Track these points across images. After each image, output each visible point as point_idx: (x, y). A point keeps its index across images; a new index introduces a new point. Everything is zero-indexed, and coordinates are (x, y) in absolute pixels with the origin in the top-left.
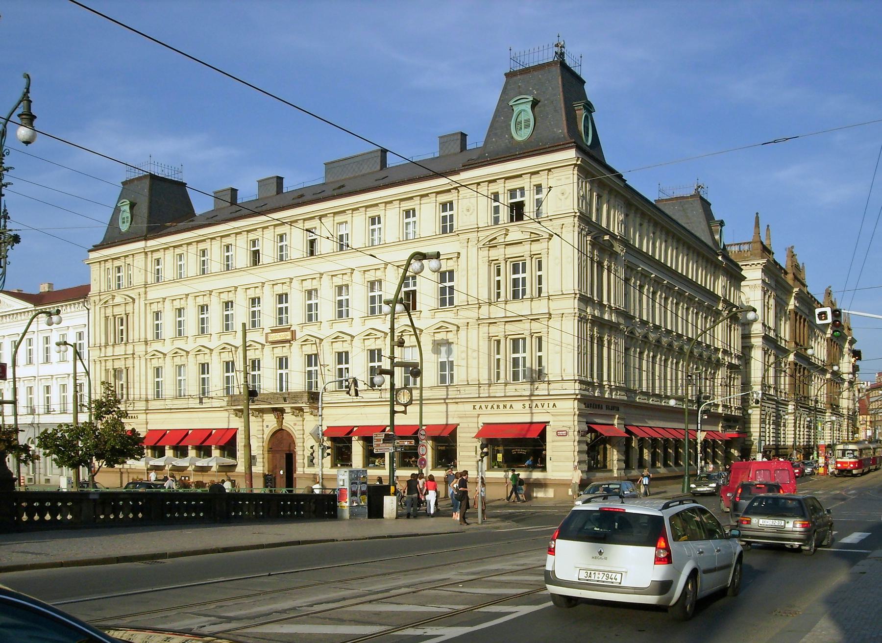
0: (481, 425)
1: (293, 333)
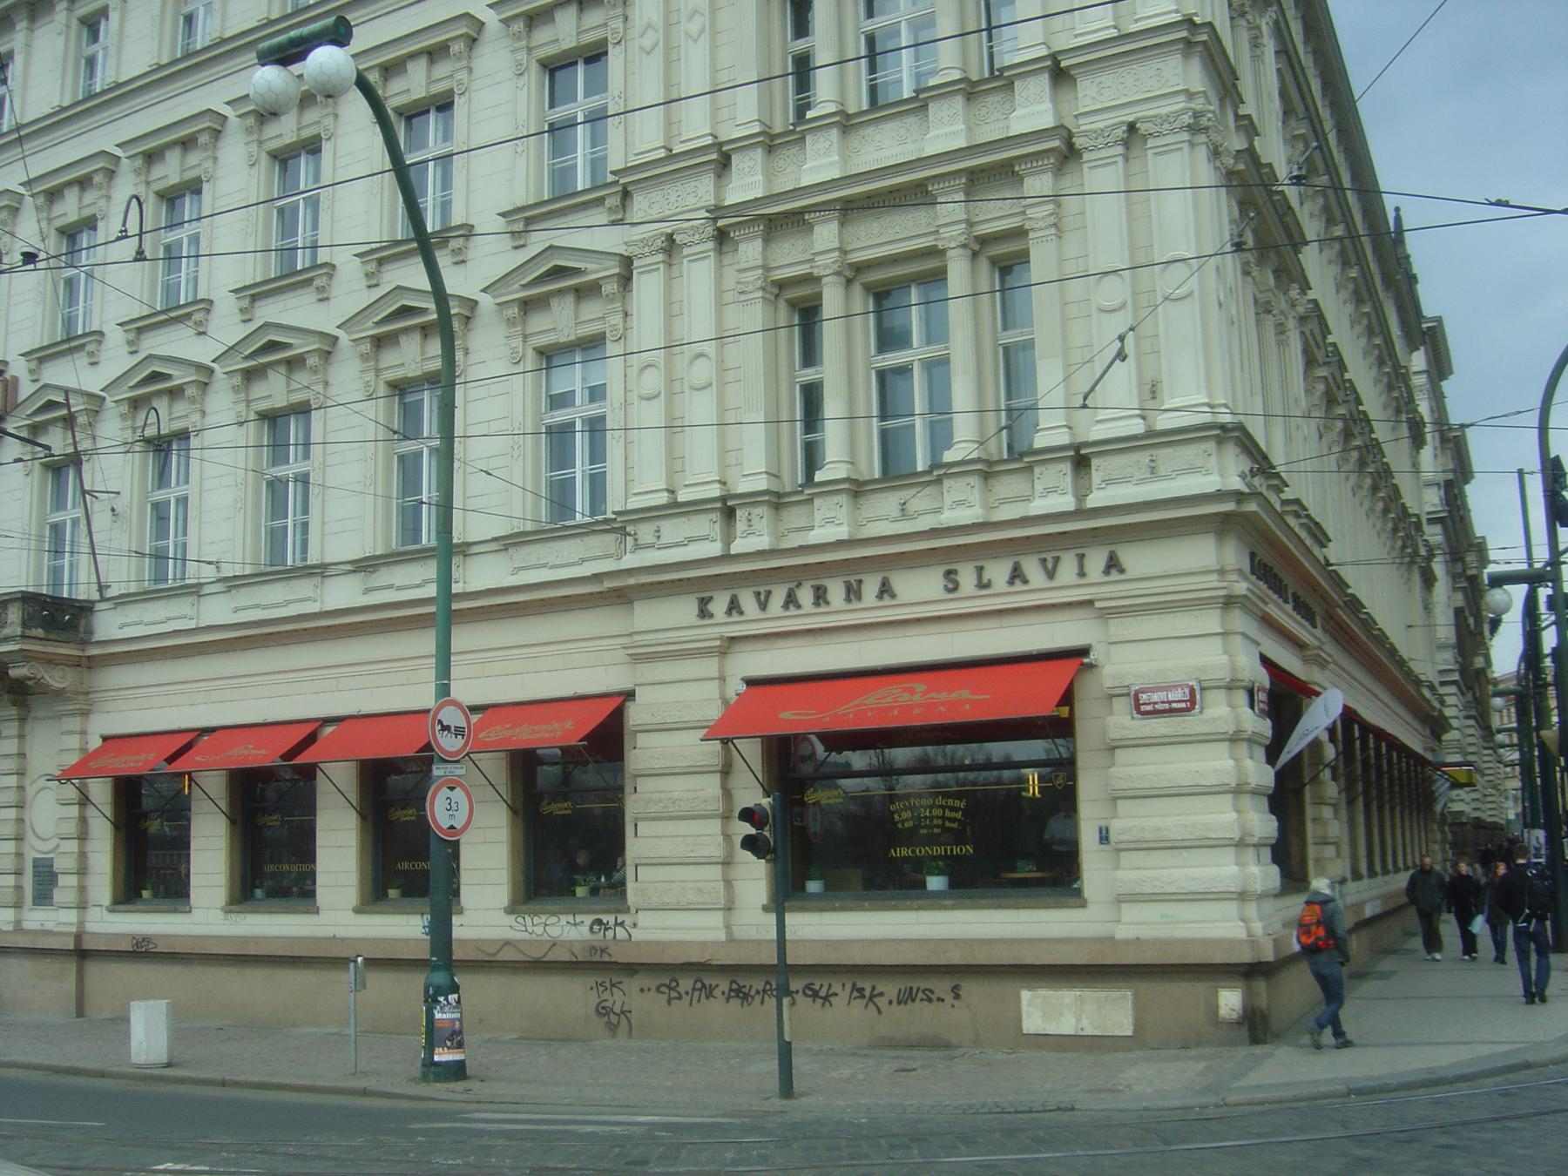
0: (736, 687)
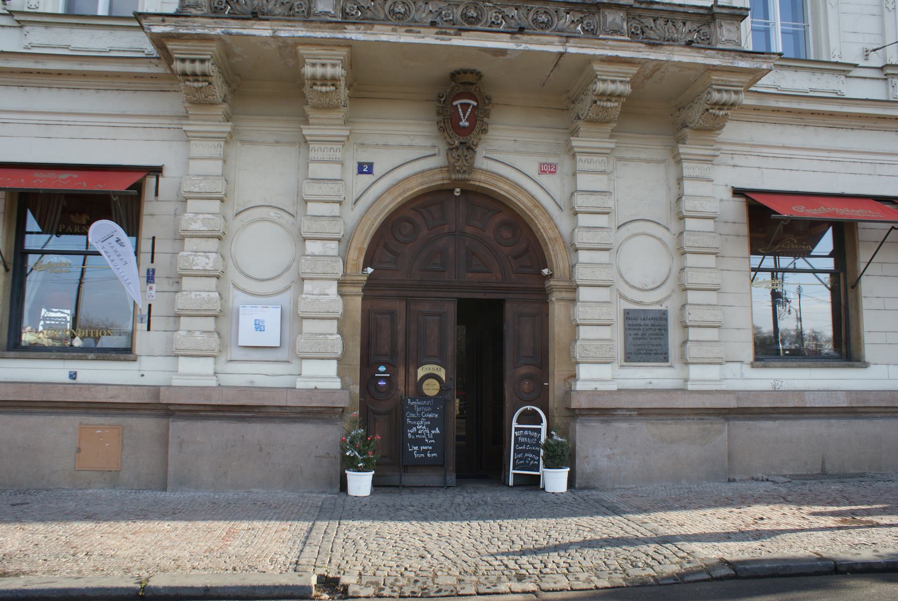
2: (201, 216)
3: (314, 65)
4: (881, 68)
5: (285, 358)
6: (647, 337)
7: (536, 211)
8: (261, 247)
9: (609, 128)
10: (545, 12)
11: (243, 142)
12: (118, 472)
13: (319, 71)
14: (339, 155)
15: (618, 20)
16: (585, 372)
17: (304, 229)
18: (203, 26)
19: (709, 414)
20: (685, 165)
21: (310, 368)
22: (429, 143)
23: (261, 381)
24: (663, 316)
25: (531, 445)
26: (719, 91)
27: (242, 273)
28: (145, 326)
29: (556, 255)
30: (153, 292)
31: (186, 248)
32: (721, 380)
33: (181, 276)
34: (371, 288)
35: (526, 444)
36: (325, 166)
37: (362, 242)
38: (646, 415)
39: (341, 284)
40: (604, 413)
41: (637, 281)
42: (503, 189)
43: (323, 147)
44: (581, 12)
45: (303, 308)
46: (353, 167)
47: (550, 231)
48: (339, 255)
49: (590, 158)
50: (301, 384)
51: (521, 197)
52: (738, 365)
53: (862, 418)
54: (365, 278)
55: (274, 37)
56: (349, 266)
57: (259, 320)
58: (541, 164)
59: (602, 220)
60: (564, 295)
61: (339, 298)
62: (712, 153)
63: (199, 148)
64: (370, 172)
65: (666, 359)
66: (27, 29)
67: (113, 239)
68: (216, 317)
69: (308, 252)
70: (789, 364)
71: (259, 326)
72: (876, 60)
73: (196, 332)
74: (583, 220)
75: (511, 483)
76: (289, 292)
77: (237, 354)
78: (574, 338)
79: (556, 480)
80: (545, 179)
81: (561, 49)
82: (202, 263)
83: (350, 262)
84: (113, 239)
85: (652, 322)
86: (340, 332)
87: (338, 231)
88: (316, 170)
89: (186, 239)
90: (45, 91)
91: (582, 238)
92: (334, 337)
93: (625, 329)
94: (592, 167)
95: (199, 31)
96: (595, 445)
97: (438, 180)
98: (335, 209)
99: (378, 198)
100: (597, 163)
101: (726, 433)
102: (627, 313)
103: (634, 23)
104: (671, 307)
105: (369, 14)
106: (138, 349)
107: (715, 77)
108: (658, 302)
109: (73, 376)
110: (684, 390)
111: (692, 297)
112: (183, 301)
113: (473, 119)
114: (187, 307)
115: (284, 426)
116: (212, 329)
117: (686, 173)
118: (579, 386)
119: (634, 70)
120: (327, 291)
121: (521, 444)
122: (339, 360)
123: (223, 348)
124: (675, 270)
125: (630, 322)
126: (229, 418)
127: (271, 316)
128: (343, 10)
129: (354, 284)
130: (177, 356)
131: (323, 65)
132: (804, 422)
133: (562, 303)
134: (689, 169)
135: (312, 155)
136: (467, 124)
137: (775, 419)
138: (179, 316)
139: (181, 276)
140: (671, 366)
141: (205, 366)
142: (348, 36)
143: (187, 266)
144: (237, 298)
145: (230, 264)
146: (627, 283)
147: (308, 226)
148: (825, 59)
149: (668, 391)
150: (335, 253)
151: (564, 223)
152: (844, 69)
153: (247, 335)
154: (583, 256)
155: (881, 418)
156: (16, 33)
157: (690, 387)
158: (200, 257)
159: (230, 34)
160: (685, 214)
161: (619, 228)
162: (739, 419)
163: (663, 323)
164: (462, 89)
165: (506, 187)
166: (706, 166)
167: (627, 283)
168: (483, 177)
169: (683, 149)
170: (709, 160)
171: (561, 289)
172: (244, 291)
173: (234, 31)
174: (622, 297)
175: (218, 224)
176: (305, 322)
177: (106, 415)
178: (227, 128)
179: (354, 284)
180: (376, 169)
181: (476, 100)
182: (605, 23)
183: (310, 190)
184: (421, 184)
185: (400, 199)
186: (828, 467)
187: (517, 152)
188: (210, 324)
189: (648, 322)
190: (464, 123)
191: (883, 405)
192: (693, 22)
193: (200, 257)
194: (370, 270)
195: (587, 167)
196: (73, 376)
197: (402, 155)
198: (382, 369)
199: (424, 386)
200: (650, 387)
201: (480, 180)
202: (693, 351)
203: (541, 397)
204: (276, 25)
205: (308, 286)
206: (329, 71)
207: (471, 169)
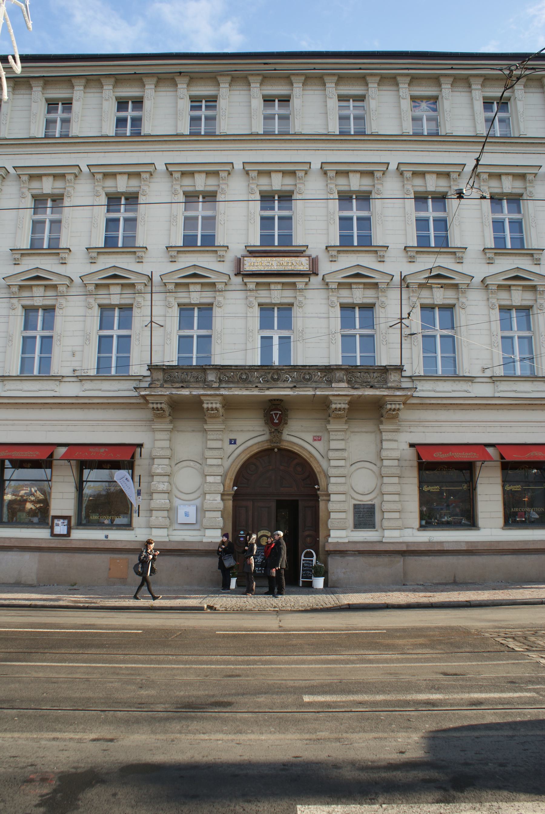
1: (314, 262)
2: (160, 466)
3: (208, 403)
4: (491, 377)
5: (198, 528)
6: (365, 516)
7: (311, 459)
8: (187, 479)
9: (344, 420)
10: (309, 373)
11: (178, 431)
12: (126, 579)
13: (210, 406)
14: (220, 437)
15: (342, 375)
16: (333, 533)
17: (206, 471)
18: (161, 391)
19: (394, 553)
20: (383, 434)
21: (209, 533)
22: (261, 429)
23: (188, 539)
24: (373, 506)
25: (309, 567)
26: (391, 404)
27: (179, 491)
28: (137, 515)
29: (321, 479)
30: (140, 500)
31: (154, 480)
32: (401, 537)
33: (153, 493)
34: (236, 497)
35: (307, 567)
36: (215, 442)
37: (232, 475)
38: (363, 553)
39: (222, 495)
40: (341, 552)
41: (360, 489)
42: (296, 449)
43: (213, 433)
44: (326, 372)
45: (206, 506)
46: (228, 442)
47: (318, 468)
48: (221, 482)
49: (336, 433)
50: (205, 540)
51: (304, 453)
52: (410, 530)
53: (476, 555)
54: (233, 492)
55: (191, 394)
56: (226, 487)
57: (186, 512)
58: (314, 436)
59: (342, 463)
60: (325, 498)
61: (221, 502)
62: (397, 427)
63: (159, 435)
64: (235, 443)
65: (374, 527)
66: (83, 382)
67: (124, 479)
68: (168, 510)
69: (208, 481)
70: (437, 529)
71: (187, 514)
72: (488, 373)
73: (159, 517)
74: (333, 463)
75: (301, 585)
76: (199, 499)
77: (177, 527)
78: (329, 517)
79: (319, 582)
80: (317, 444)
81: (313, 393)
82: (163, 487)
83: (226, 485)
84: (124, 479)
85: (367, 510)
86: (222, 517)
87: (220, 471)
88: (211, 444)
89: (155, 477)
90: (91, 411)
91: (332, 472)
92: (219, 519)
93: (354, 513)
94: (338, 437)
95: (160, 393)
96: (337, 568)
97: (266, 446)
98: (219, 462)
99: (239, 455)
100: (340, 435)
101: (402, 563)
102: (355, 506)
103: (349, 376)
104: (376, 502)
105: (231, 380)
106: (134, 524)
107: (387, 399)
108: (370, 500)
109: (107, 537)
110: (381, 542)
111: (386, 498)
112: (154, 504)
113: (280, 419)
114: (156, 507)
115: (198, 558)
116: (166, 516)
117: (384, 438)
118: (330, 540)
119: (349, 398)
120: (216, 499)
121: (305, 567)
122: (222, 529)
123: (171, 524)
124: (379, 484)
125: (356, 510)
126: (174, 555)
127: (192, 511)
128: (219, 378)
129: (228, 495)
130: (151, 528)
131: (212, 403)
132: (445, 557)
133: (324, 502)
134: (385, 436)
135: (209, 437)
136: (277, 421)
137: (429, 556)
138: (152, 510)
139: (153, 493)
140: (377, 531)
141: (164, 532)
142: (221, 393)
143: (155, 488)
144: (177, 502)
145: (174, 487)
146: (355, 491)
147: (207, 470)
148: (461, 375)
149: (372, 542)
150: (220, 481)
151: (324, 463)
152: (470, 379)
153: (181, 518)
154: (333, 480)
155: (486, 555)
156: (78, 384)
157: (384, 541)
158: (160, 484)
159: (172, 394)
160: (383, 458)
161: (351, 465)
162: (410, 556)
163: (373, 510)
164: (274, 407)
165: (297, 448)
166: (394, 434)
167: (355, 491)
168: (286, 444)
169: (381, 427)
170: (397, 431)
171: (323, 495)
172: (180, 499)
173: (174, 392)
174: (353, 498)
175: (168, 470)
176: (207, 513)
177: (121, 554)
178: (171, 426)
179: (228, 495)
180: (237, 442)
181: (280, 411)
182: (335, 377)
183: (208, 453)
184: (258, 448)
185: (249, 456)
186: (457, 579)
187: (302, 431)
188: (165, 514)
189: (365, 510)
190: (276, 421)
191: (486, 548)
192: (378, 372)
193: (160, 484)
194: (236, 488)
195: (335, 438)
196: (107, 537)
197: (249, 435)
198: (242, 532)
199: (261, 540)
200: (365, 540)
201: (285, 445)
202: (386, 524)
203: (315, 545)
204: (191, 390)
205: (208, 497)
206: (214, 406)
207: (281, 440)
